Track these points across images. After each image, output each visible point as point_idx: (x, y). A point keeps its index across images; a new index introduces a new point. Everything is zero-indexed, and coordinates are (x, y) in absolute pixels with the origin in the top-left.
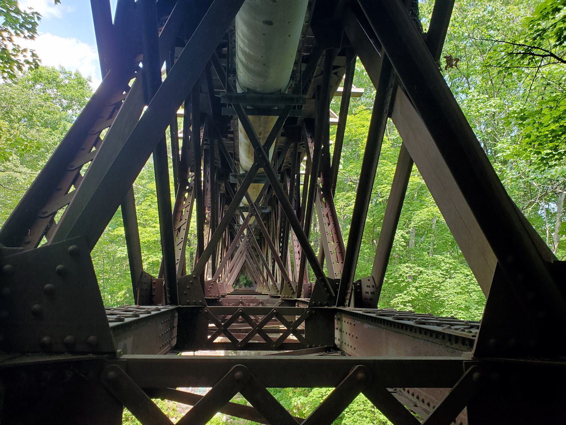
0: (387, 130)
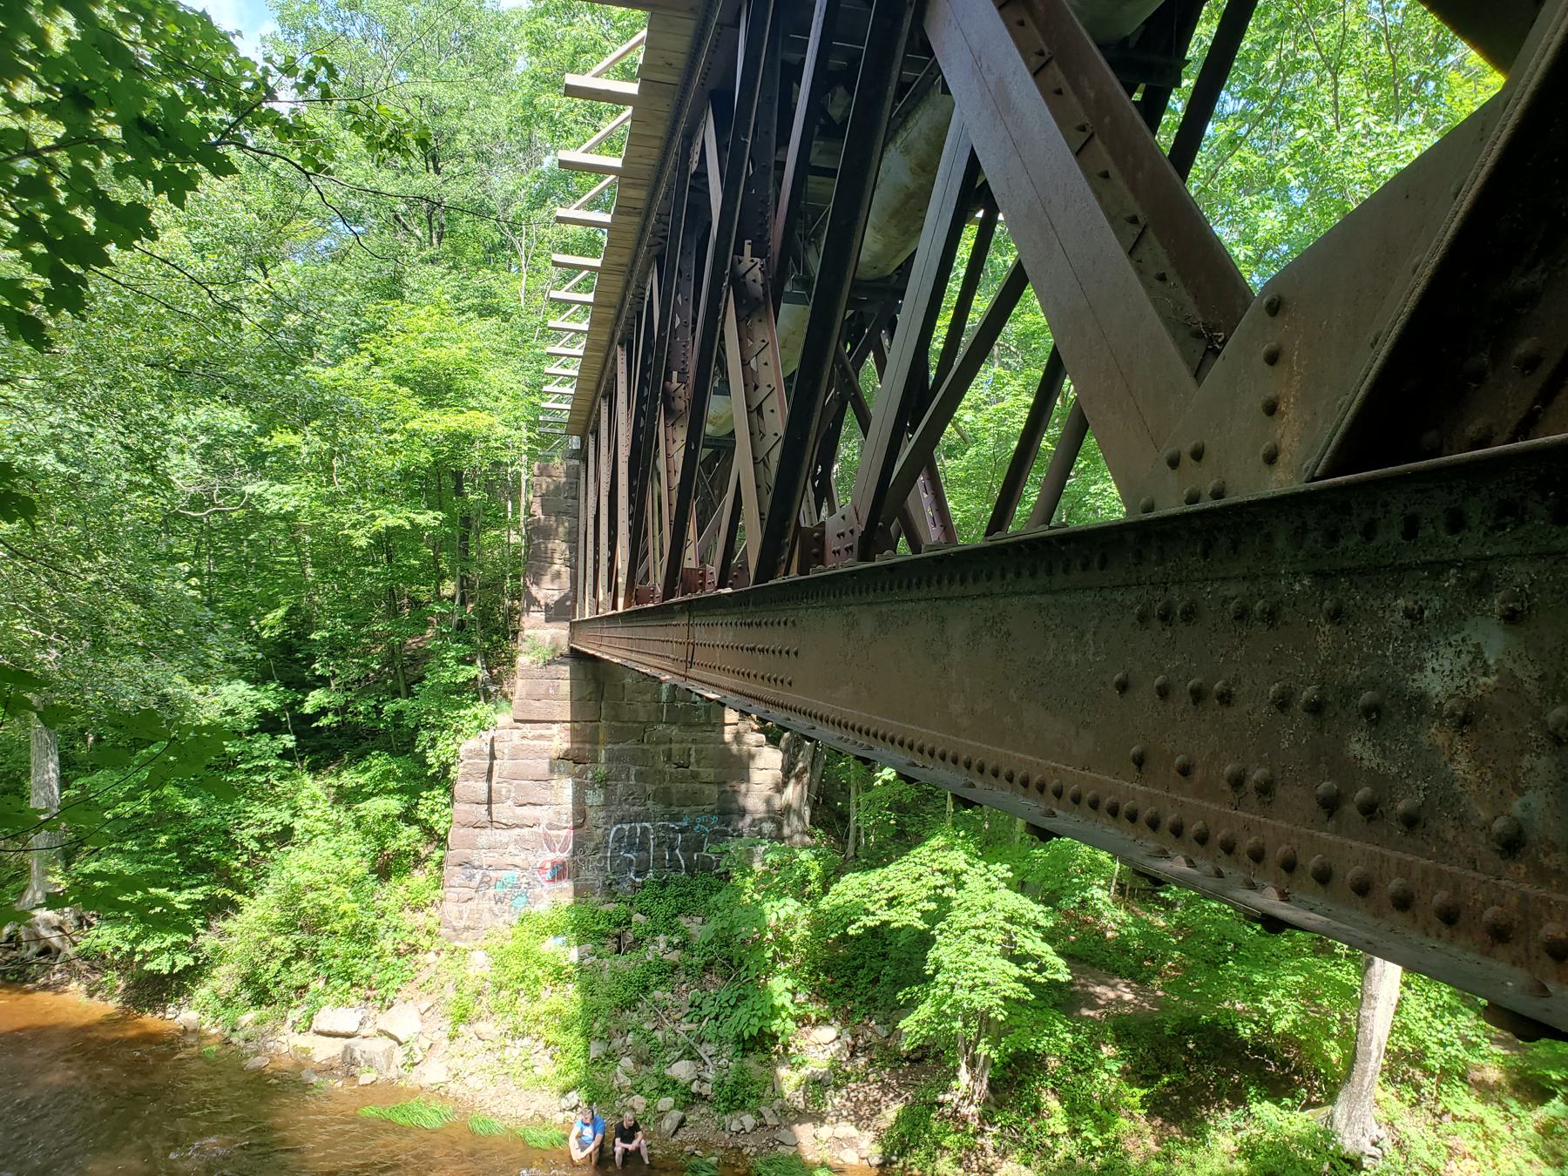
0: (1061, 511)
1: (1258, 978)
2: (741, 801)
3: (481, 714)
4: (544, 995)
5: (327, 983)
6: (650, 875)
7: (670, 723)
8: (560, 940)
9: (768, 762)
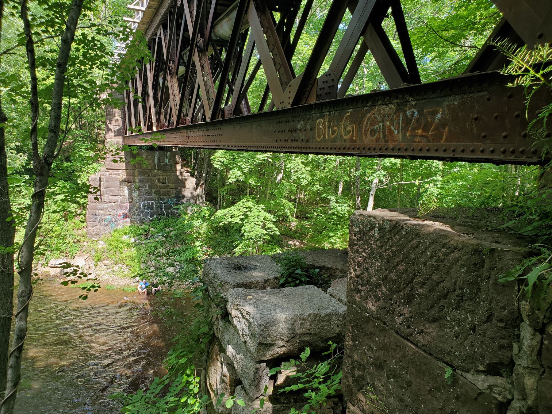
1: (331, 234)
2: (183, 193)
3: (95, 167)
4: (124, 252)
5: (51, 252)
6: (155, 217)
7: (159, 169)
8: (127, 236)
9: (191, 182)
